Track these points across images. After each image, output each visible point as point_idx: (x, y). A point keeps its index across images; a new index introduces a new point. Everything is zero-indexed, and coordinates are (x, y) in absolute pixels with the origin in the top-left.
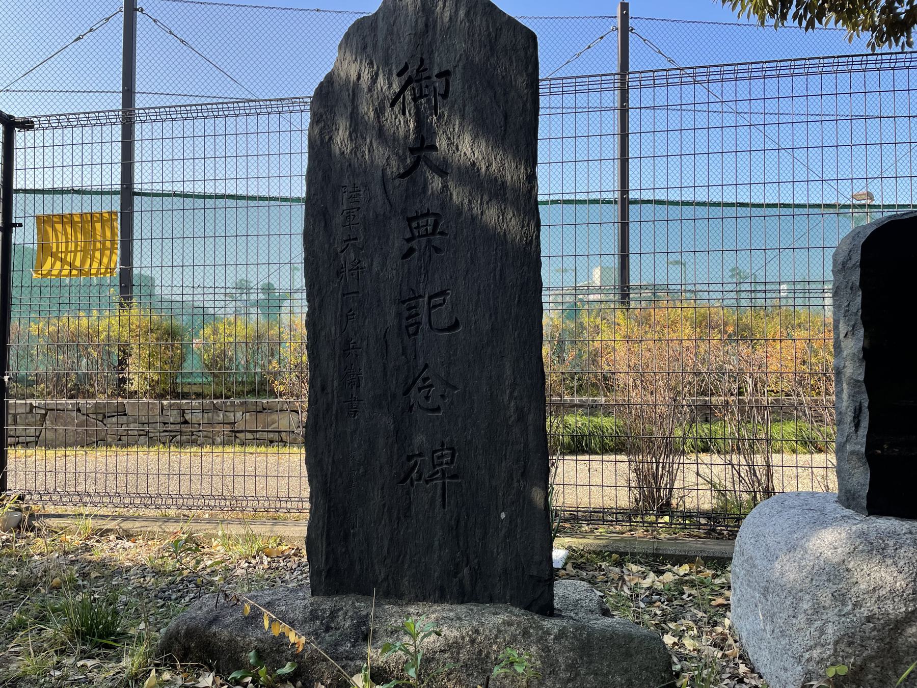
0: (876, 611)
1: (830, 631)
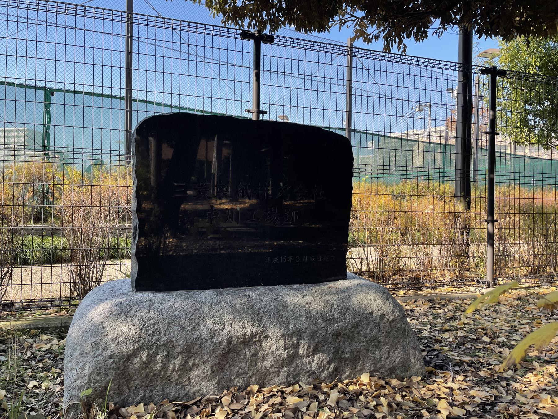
0: (116, 351)
1: (87, 368)
